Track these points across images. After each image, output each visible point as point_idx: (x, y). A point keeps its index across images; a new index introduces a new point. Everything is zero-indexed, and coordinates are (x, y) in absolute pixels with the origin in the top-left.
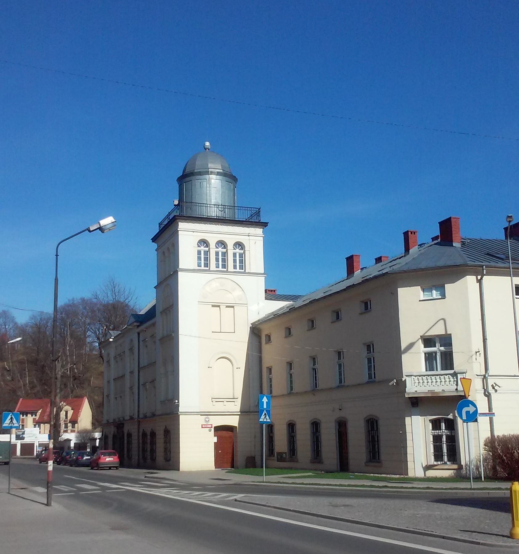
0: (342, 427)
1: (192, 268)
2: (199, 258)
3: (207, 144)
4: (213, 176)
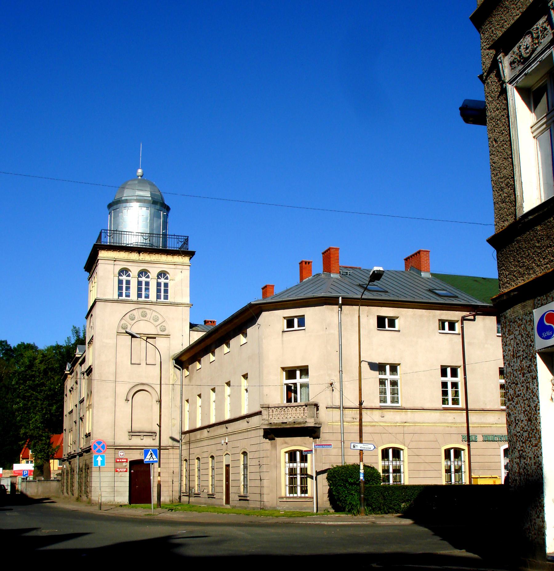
1: (110, 297)
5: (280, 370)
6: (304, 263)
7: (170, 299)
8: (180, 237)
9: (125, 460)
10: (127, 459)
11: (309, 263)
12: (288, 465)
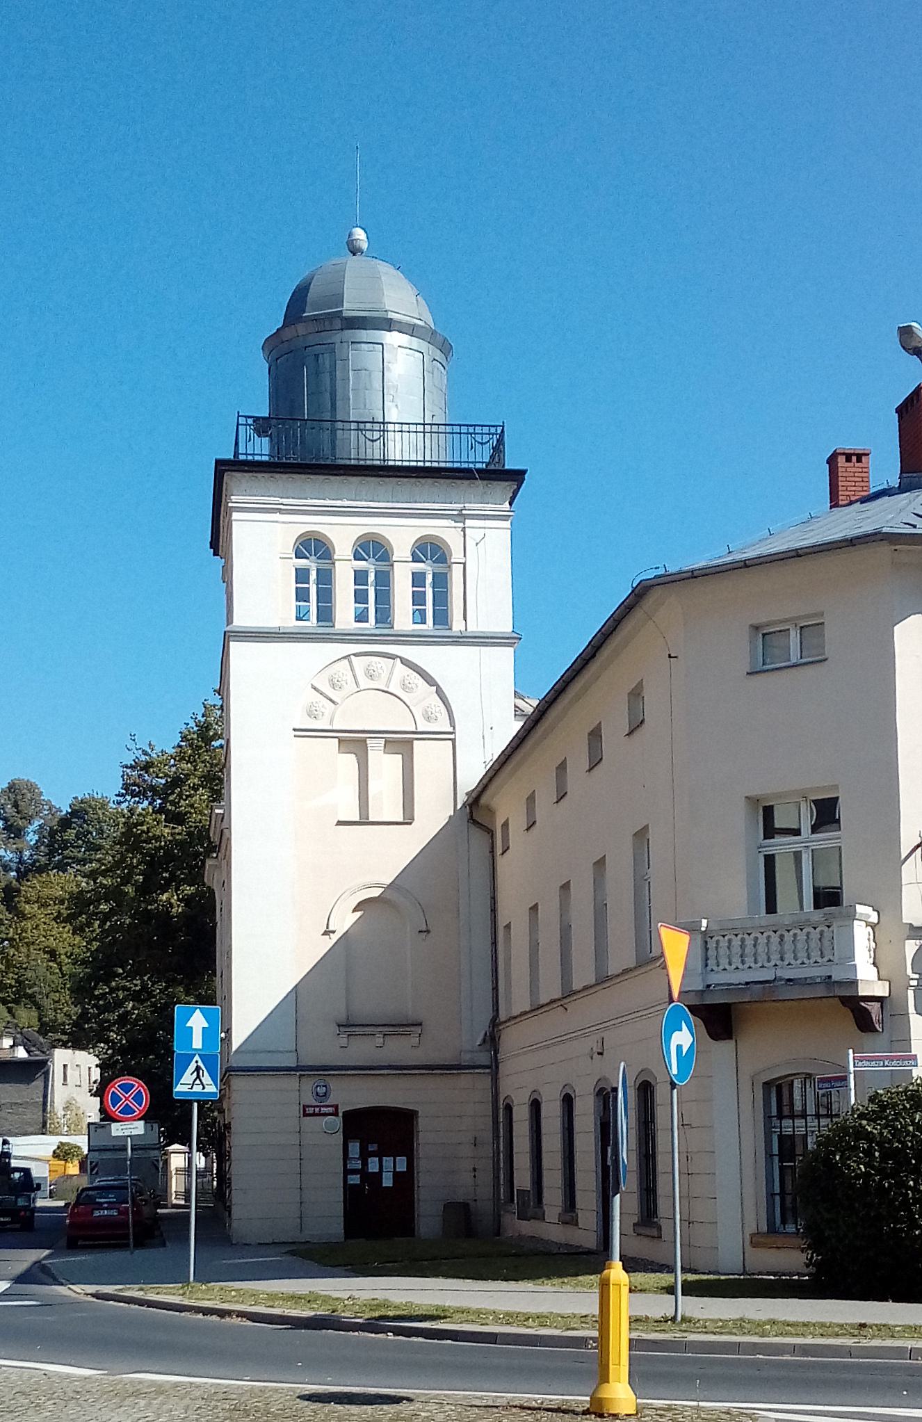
2: (302, 595)
3: (360, 234)
4: (393, 339)
5: (742, 803)
6: (841, 460)
8: (478, 430)
9: (331, 1110)
10: (336, 1107)
11: (859, 457)
12: (775, 1122)
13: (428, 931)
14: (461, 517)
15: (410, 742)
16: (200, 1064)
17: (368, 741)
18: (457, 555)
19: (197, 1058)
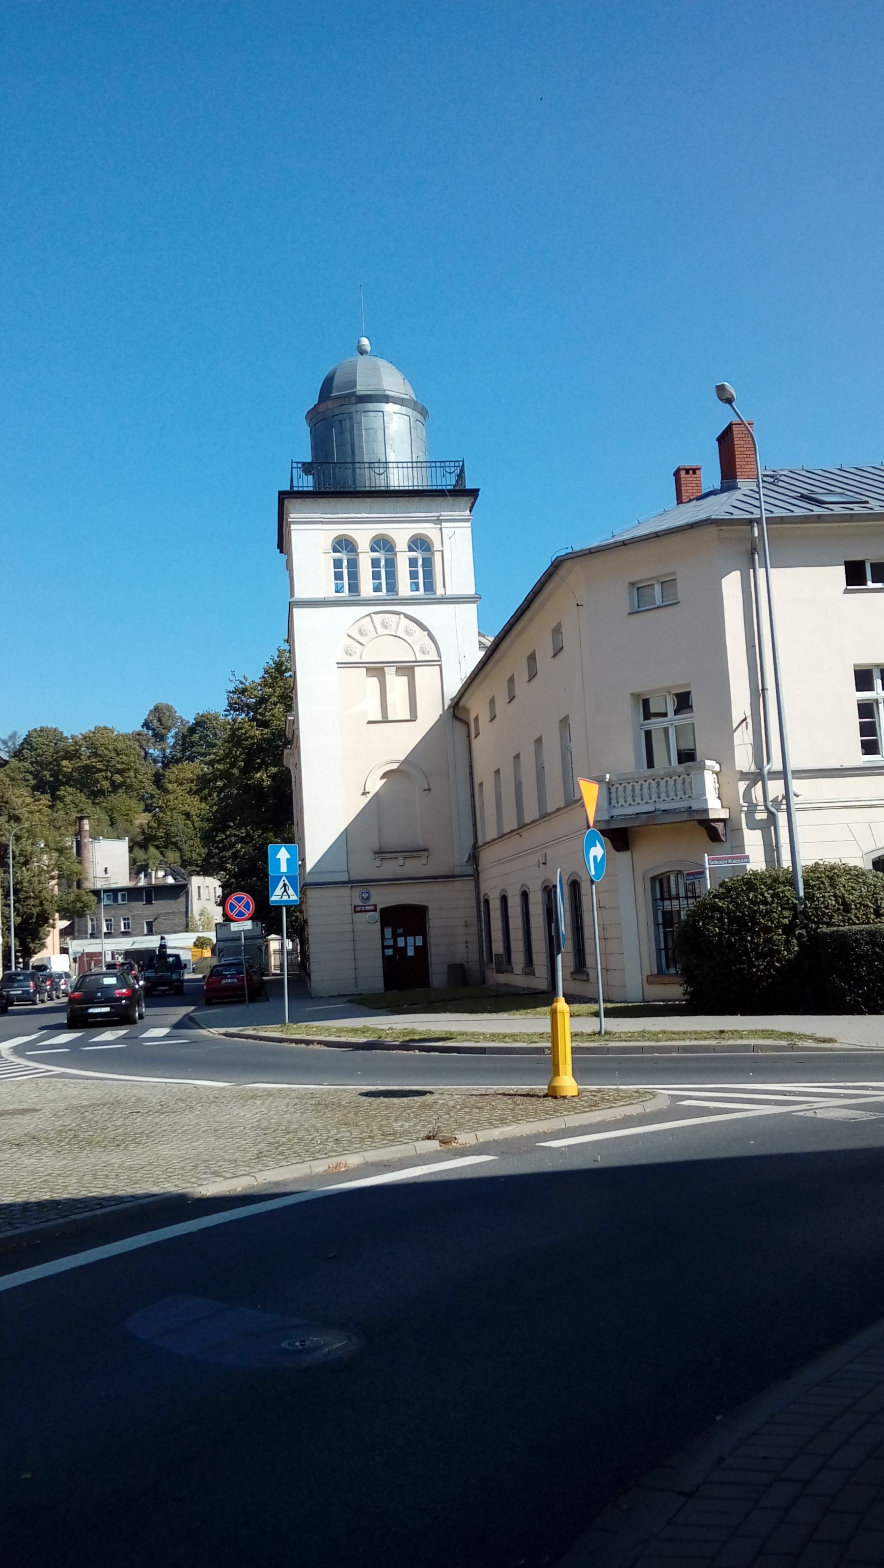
0: (549, 891)
1: (320, 595)
2: (338, 576)
3: (365, 341)
6: (683, 473)
7: (440, 591)
9: (372, 908)
10: (375, 906)
11: (694, 471)
13: (429, 790)
14: (438, 521)
15: (412, 668)
16: (286, 882)
17: (386, 669)
18: (437, 546)
19: (284, 878)
